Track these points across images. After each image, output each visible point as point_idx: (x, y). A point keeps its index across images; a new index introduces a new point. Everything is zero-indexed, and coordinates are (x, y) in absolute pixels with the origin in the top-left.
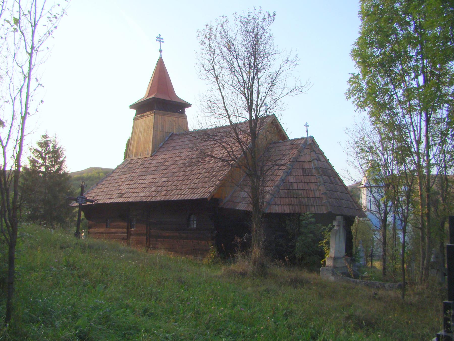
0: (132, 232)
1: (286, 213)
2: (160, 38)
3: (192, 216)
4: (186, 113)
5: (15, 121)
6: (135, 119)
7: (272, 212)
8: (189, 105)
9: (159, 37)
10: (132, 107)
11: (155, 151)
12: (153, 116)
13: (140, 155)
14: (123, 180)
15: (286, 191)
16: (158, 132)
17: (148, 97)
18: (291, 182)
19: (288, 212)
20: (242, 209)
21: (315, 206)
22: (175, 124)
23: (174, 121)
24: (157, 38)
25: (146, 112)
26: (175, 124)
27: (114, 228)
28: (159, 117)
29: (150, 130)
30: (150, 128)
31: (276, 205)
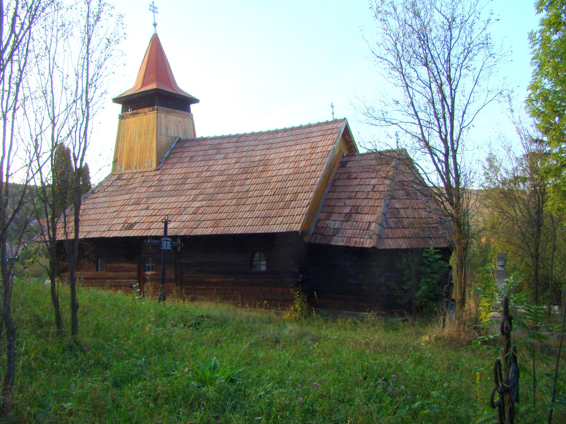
0: (148, 277)
1: (403, 249)
2: (153, 7)
3: (257, 254)
4: (192, 111)
5: (81, 122)
6: (121, 117)
7: (386, 248)
8: (196, 101)
9: (152, 5)
10: (116, 100)
11: (160, 163)
12: (155, 115)
13: (136, 168)
14: (120, 203)
15: (394, 220)
16: (163, 136)
17: (142, 87)
18: (398, 208)
19: (405, 247)
20: (340, 244)
21: (433, 239)
22: (180, 126)
23: (180, 122)
24: (150, 6)
25: (140, 108)
26: (180, 126)
27: (111, 271)
28: (163, 116)
29: (150, 133)
30: (151, 131)
31: (388, 238)
